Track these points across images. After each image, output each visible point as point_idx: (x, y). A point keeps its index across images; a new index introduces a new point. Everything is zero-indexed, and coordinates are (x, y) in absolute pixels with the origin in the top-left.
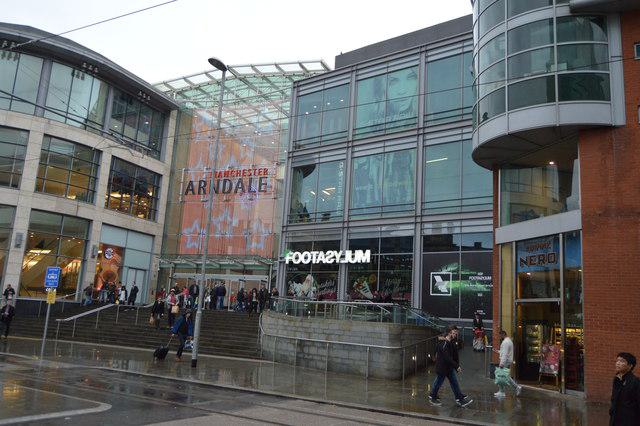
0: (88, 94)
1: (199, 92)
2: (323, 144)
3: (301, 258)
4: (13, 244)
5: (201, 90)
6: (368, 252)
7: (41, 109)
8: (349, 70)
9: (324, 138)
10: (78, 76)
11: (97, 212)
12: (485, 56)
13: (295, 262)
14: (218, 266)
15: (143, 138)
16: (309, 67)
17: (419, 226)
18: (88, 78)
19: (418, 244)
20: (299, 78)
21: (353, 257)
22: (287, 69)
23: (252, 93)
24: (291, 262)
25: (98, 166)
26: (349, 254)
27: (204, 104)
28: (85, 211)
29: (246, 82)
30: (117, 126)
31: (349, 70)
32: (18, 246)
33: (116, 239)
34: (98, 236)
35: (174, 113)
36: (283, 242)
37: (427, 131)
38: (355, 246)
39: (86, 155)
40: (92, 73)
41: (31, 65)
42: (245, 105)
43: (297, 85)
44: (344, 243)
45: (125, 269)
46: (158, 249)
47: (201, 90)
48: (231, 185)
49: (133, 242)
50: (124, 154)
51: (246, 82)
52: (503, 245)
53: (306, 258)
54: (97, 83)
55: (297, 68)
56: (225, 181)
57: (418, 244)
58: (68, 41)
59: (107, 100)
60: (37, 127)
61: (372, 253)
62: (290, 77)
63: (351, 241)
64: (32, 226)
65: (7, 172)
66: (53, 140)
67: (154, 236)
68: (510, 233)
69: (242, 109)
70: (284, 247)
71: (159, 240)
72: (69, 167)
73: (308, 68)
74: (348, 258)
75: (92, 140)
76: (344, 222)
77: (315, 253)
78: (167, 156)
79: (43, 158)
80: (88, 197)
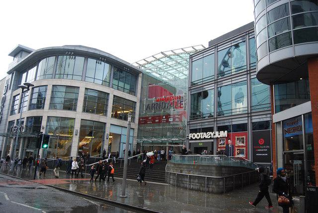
0: (104, 70)
1: (151, 65)
2: (204, 82)
3: (196, 136)
4: (74, 134)
5: (160, 61)
6: (226, 132)
7: (84, 77)
8: (214, 47)
9: (204, 80)
10: (99, 63)
11: (108, 119)
12: (261, 36)
13: (193, 138)
14: (151, 141)
15: (127, 87)
16: (197, 48)
17: (250, 117)
18: (103, 63)
19: (250, 127)
20: (192, 54)
21: (219, 134)
22: (187, 50)
23: (174, 62)
24: (191, 138)
25: (108, 100)
26: (217, 133)
27: (153, 70)
28: (102, 119)
29: (171, 58)
30: (116, 82)
31: (214, 47)
32: (76, 135)
33: (117, 131)
34: (109, 130)
35: (141, 75)
36: (187, 129)
37: (251, 71)
38: (220, 129)
39: (103, 95)
40: (104, 61)
41: (80, 60)
42: (171, 68)
43: (191, 57)
44: (215, 128)
45: (121, 144)
46: (136, 135)
47: (160, 61)
48: (165, 105)
49: (124, 132)
50: (120, 94)
51: (171, 58)
52: (277, 123)
53: (198, 136)
54: (107, 66)
55: (192, 49)
56: (163, 103)
57: (250, 127)
58: (95, 49)
59: (110, 75)
60: (82, 86)
61: (228, 132)
62: (189, 54)
63: (218, 127)
64: (82, 126)
65: (71, 105)
66: (89, 90)
67: (134, 129)
68: (279, 117)
69: (180, 68)
70: (188, 131)
71: (136, 131)
72: (97, 103)
73: (187, 51)
74: (217, 136)
75: (105, 89)
76: (214, 118)
77: (202, 133)
78: (138, 94)
79: (85, 98)
80: (86, 110)
